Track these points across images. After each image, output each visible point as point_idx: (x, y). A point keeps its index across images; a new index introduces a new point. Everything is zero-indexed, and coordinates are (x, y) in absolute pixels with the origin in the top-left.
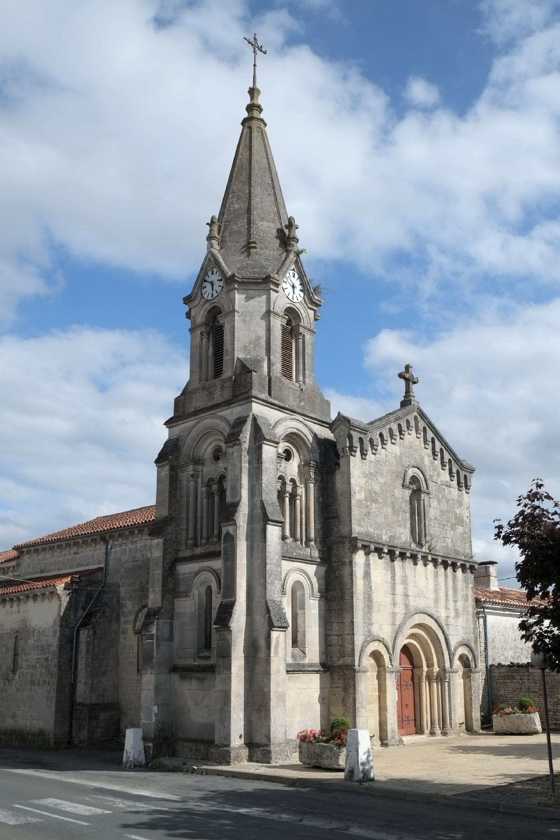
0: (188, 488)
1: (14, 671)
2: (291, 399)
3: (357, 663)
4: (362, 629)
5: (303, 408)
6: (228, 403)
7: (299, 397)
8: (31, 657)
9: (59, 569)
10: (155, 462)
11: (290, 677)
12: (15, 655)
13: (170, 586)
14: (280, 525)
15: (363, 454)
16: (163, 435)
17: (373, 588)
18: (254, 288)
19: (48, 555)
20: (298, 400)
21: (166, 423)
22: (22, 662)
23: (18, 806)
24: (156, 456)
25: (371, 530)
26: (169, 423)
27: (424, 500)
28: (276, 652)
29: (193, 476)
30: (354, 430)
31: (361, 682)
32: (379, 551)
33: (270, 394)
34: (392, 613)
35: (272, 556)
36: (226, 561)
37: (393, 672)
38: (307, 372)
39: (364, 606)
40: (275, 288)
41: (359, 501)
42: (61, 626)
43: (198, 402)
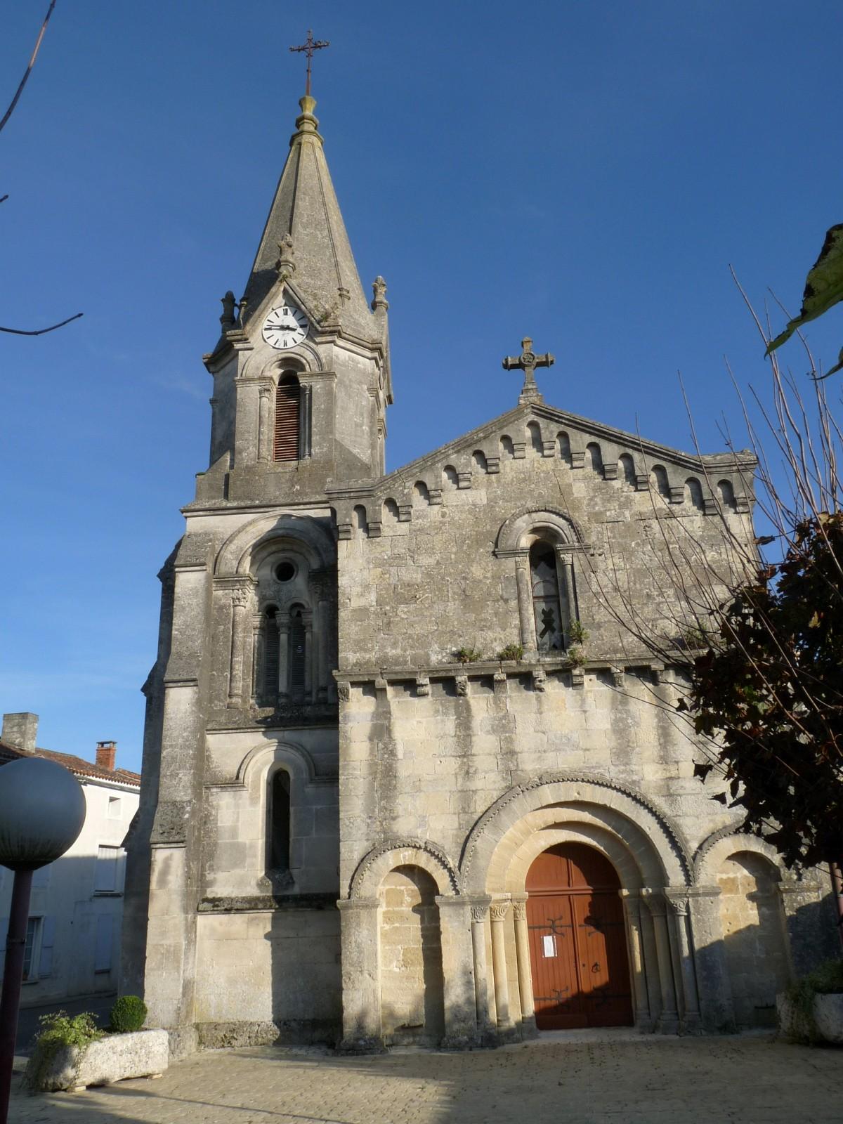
3: (344, 891)
4: (364, 829)
5: (299, 493)
11: (253, 919)
14: (192, 684)
15: (371, 529)
17: (400, 755)
18: (228, 360)
25: (392, 652)
27: (572, 565)
28: (163, 882)
30: (339, 499)
31: (358, 925)
32: (410, 685)
34: (462, 791)
37: (461, 904)
39: (371, 788)
40: (246, 346)
41: (363, 612)
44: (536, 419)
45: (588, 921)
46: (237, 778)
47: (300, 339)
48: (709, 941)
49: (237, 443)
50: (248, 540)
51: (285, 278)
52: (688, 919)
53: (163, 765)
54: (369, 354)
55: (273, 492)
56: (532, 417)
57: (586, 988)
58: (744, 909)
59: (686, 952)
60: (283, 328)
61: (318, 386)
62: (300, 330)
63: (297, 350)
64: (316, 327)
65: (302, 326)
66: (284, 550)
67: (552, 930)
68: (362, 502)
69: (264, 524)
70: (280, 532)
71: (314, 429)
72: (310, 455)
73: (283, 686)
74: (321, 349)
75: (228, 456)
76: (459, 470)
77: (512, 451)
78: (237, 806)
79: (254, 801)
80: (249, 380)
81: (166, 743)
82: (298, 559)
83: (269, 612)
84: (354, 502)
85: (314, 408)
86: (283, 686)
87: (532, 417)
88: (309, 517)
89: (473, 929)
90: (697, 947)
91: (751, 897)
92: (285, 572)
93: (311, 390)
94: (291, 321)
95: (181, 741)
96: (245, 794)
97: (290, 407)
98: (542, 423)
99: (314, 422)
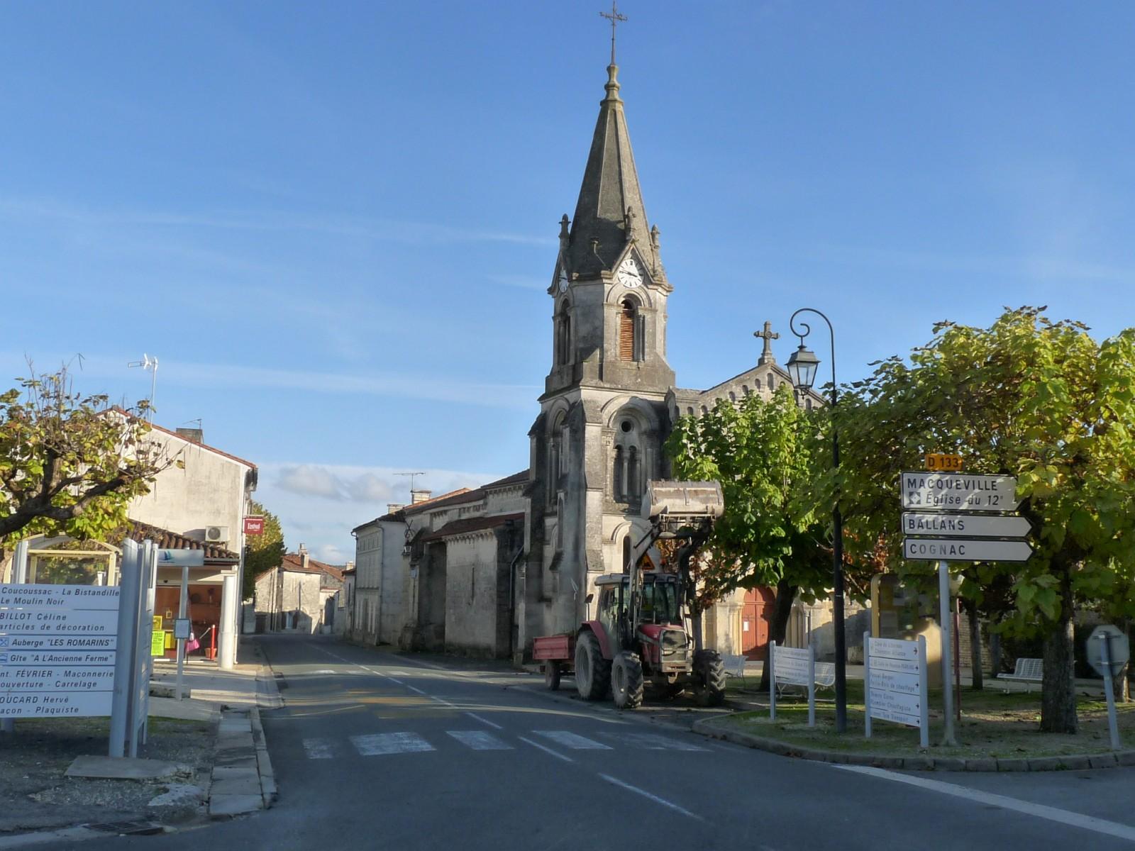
0: (551, 455)
1: (473, 596)
2: (626, 378)
5: (640, 384)
6: (568, 389)
7: (635, 375)
8: (482, 586)
9: (512, 510)
10: (530, 434)
12: (473, 584)
13: (538, 536)
16: (536, 410)
19: (505, 496)
20: (633, 378)
21: (540, 400)
22: (477, 591)
23: (497, 726)
24: (530, 429)
26: (542, 399)
29: (554, 446)
33: (601, 378)
35: (592, 516)
36: (559, 519)
38: (646, 350)
42: (498, 561)
43: (556, 385)
44: (772, 372)
45: (762, 616)
46: (612, 539)
47: (640, 283)
48: (816, 627)
49: (605, 345)
50: (613, 408)
51: (633, 242)
52: (809, 618)
53: (587, 531)
54: (665, 293)
55: (627, 381)
56: (770, 371)
57: (759, 645)
58: (827, 615)
59: (807, 631)
60: (630, 274)
61: (648, 317)
62: (639, 277)
63: (638, 290)
64: (648, 277)
65: (640, 275)
66: (627, 414)
67: (748, 619)
68: (692, 406)
69: (623, 399)
70: (631, 406)
71: (646, 345)
72: (644, 360)
73: (625, 492)
74: (650, 292)
75: (598, 352)
76: (736, 395)
77: (759, 387)
78: (611, 553)
79: (619, 551)
80: (611, 305)
81: (588, 520)
82: (634, 420)
83: (619, 448)
84: (688, 405)
85: (646, 330)
86: (625, 492)
87: (770, 371)
88: (646, 400)
89: (729, 617)
90: (812, 629)
91: (830, 610)
92: (626, 427)
93: (644, 317)
94: (634, 270)
95: (595, 520)
96: (615, 547)
97: (629, 324)
98: (774, 375)
99: (646, 340)
